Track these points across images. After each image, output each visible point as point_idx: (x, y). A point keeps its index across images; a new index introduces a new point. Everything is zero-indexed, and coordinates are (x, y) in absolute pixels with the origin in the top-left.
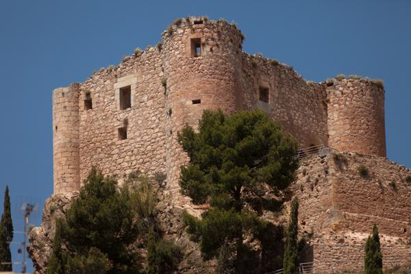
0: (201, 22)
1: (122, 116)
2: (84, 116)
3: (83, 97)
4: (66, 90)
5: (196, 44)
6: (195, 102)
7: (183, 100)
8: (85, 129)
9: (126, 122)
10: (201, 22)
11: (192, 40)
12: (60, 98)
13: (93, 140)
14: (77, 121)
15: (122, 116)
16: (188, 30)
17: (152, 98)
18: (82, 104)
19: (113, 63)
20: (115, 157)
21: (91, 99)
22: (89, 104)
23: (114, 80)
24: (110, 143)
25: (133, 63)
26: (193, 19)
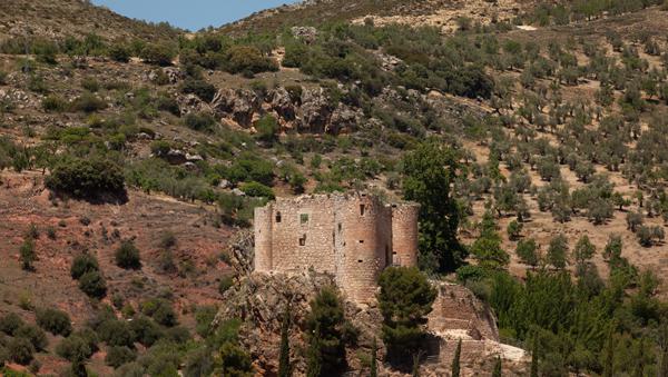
2: (275, 225)
3: (275, 214)
5: (362, 206)
9: (305, 235)
14: (271, 228)
18: (274, 218)
22: (279, 219)
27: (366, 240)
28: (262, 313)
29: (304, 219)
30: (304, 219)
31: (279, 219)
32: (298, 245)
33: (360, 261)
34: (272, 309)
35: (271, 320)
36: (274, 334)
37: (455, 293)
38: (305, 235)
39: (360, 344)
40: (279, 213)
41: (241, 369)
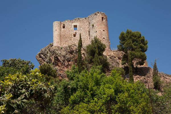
0: (103, 14)
1: (75, 31)
2: (63, 29)
3: (62, 25)
4: (59, 22)
5: (103, 18)
6: (103, 31)
7: (100, 30)
8: (63, 32)
9: (76, 33)
10: (103, 14)
11: (102, 17)
12: (56, 25)
13: (66, 35)
14: (61, 30)
15: (75, 31)
16: (101, 15)
17: (84, 29)
18: (62, 27)
19: (71, 18)
20: (72, 40)
21: (65, 26)
22: (64, 27)
23: (72, 23)
24: (71, 37)
25: (78, 20)
26: (102, 13)
27: (105, 31)
28: (59, 58)
29: (75, 26)
30: (75, 26)
31: (64, 27)
32: (73, 36)
33: (104, 38)
34: (64, 57)
35: (64, 61)
36: (66, 68)
37: (94, 25)
38: (76, 33)
39: (110, 69)
40: (64, 25)
41: (52, 76)
